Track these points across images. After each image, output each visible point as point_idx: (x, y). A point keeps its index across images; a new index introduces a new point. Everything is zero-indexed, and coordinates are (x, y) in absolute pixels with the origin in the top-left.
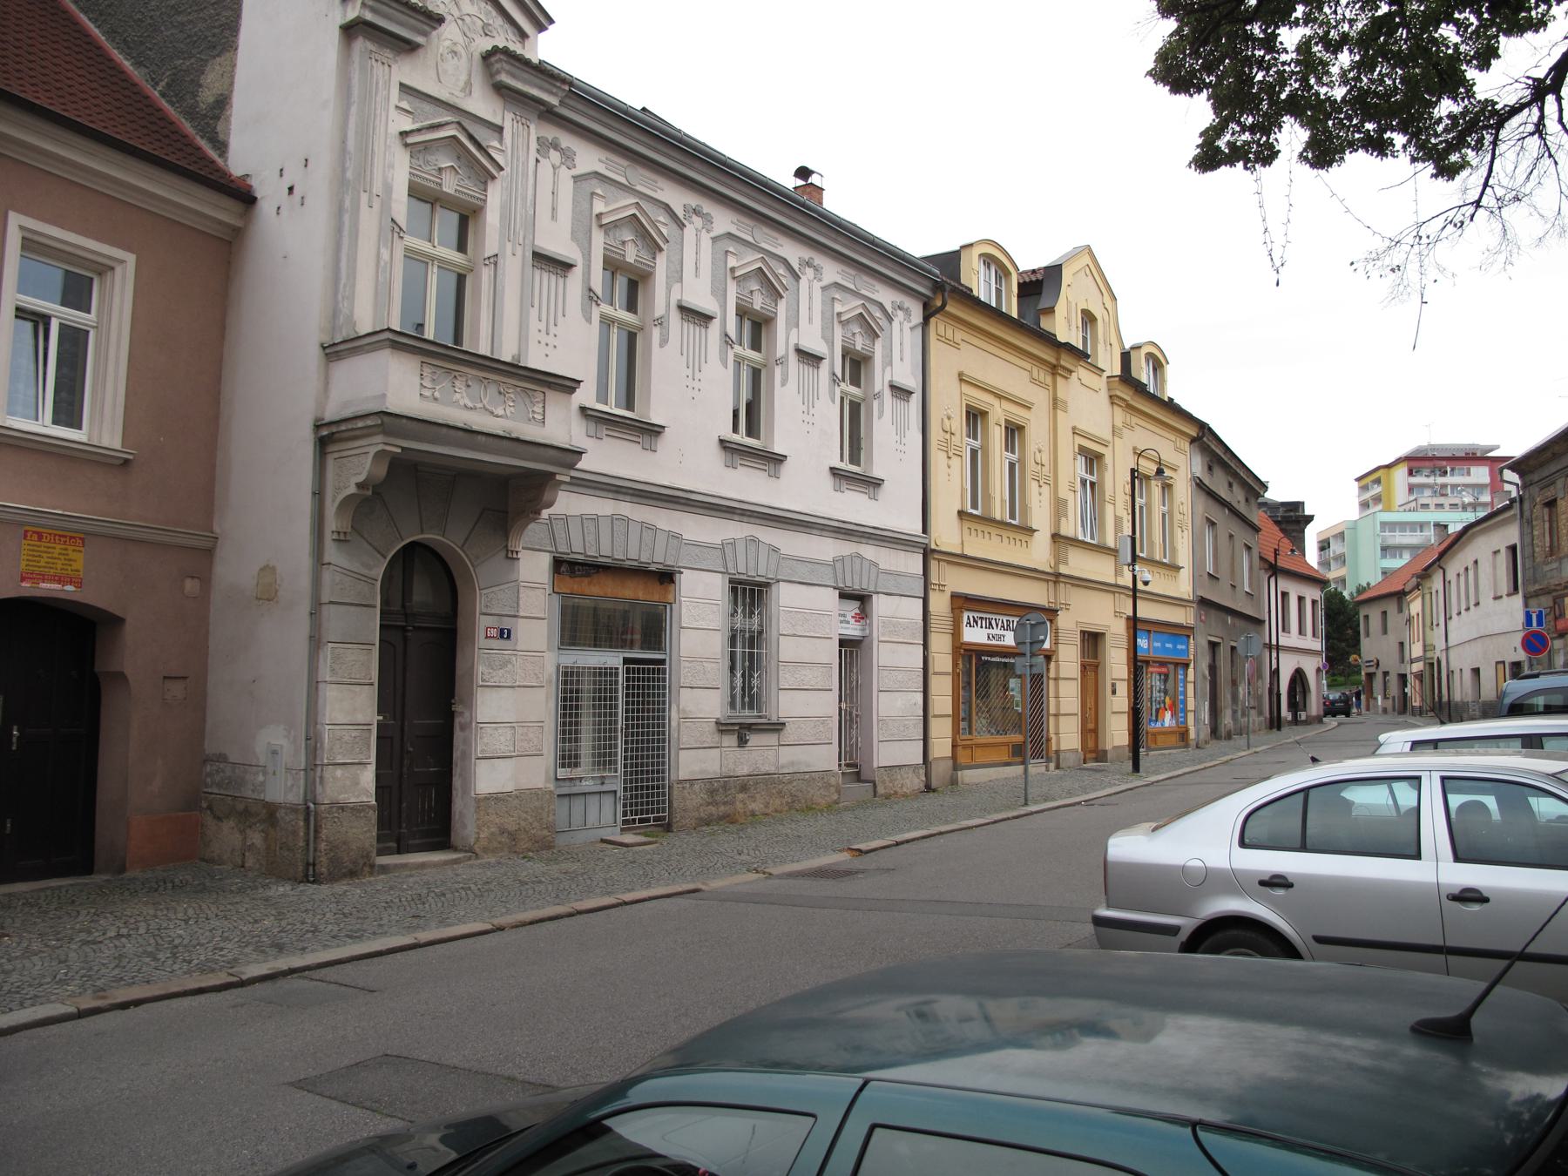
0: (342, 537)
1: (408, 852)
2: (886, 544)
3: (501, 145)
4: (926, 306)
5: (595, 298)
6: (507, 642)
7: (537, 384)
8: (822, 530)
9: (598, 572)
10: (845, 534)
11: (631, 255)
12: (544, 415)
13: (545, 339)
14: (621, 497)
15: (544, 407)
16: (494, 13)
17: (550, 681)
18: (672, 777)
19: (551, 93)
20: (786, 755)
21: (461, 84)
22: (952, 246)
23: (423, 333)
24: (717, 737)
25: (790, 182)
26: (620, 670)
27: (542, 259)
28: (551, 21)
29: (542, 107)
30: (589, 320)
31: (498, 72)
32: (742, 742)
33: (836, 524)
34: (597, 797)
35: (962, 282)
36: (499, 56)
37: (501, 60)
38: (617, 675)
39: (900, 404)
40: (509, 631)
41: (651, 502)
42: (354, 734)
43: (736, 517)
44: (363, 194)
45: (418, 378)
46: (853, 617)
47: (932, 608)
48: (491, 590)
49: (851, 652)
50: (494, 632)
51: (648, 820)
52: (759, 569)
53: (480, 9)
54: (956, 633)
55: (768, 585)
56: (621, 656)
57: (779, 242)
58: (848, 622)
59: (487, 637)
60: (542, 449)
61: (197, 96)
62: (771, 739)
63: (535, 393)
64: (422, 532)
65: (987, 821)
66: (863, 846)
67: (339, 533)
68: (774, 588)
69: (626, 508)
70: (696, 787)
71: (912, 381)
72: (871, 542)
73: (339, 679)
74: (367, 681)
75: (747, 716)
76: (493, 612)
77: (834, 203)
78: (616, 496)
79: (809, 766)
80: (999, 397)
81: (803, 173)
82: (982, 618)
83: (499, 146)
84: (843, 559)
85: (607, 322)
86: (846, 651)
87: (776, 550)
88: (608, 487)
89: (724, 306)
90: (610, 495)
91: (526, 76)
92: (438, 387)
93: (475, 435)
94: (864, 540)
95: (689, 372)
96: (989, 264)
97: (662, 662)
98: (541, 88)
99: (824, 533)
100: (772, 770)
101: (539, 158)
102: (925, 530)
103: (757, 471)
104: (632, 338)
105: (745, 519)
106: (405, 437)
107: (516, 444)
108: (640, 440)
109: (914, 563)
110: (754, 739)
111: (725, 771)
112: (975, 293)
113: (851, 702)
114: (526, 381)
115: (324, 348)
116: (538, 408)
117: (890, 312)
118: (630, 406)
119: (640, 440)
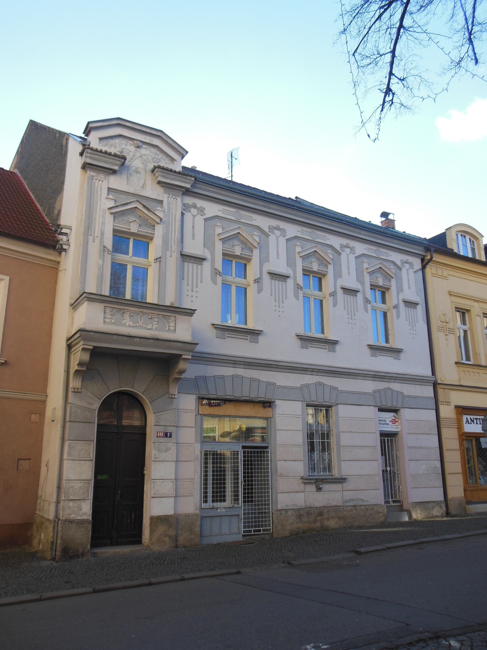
0: (76, 390)
1: (117, 545)
2: (223, 364)
3: (162, 208)
4: (423, 260)
5: (300, 288)
6: (170, 439)
7: (171, 313)
8: (365, 377)
9: (225, 403)
10: (379, 378)
11: (315, 267)
12: (175, 327)
13: (190, 294)
14: (237, 366)
15: (175, 324)
16: (158, 153)
17: (198, 458)
18: (274, 507)
19: (186, 182)
20: (348, 495)
21: (141, 185)
22: (442, 231)
23: (125, 297)
24: (302, 486)
25: (377, 221)
26: (240, 452)
27: (185, 257)
28: (187, 152)
29: (183, 190)
30: (215, 283)
31: (158, 177)
32: (319, 489)
33: (373, 373)
34: (228, 518)
35: (448, 247)
36: (157, 169)
37: (157, 171)
38: (238, 454)
39: (411, 311)
40: (171, 434)
41: (255, 368)
42: (80, 485)
43: (309, 373)
44: (90, 237)
45: (103, 314)
46: (390, 421)
47: (442, 414)
48: (160, 414)
49: (391, 440)
50: (162, 434)
51: (259, 531)
52: (326, 399)
53: (150, 152)
54: (460, 427)
55: (330, 407)
56: (241, 445)
57: (327, 238)
58: (388, 424)
59: (157, 437)
60: (172, 343)
61: (54, 212)
62: (338, 487)
63: (170, 317)
64: (121, 387)
65: (463, 536)
66: (362, 550)
67: (74, 388)
68: (334, 408)
69: (240, 371)
70: (290, 513)
71: (419, 299)
72: (398, 381)
73: (72, 458)
74: (89, 459)
75: (323, 475)
76: (161, 424)
77: (399, 227)
78: (234, 365)
79: (363, 501)
80: (475, 301)
81: (385, 215)
82: (476, 419)
83: (161, 210)
84: (379, 391)
85: (306, 298)
86: (388, 440)
87: (335, 388)
88: (327, 371)
89: (295, 271)
90: (231, 365)
91: (172, 177)
92: (114, 318)
93: (133, 338)
94: (392, 381)
95: (277, 303)
96: (465, 237)
97: (266, 447)
98: (180, 181)
99: (366, 378)
100: (340, 504)
101: (184, 212)
102: (433, 373)
103: (239, 340)
104: (385, 314)
105: (315, 373)
106: (95, 341)
107: (157, 341)
108: (393, 356)
109: (428, 391)
110: (326, 487)
111: (308, 505)
112: (456, 251)
113: (394, 466)
114: (165, 312)
115: (72, 305)
116: (172, 324)
117: (400, 266)
118: (387, 341)
119: (393, 356)
